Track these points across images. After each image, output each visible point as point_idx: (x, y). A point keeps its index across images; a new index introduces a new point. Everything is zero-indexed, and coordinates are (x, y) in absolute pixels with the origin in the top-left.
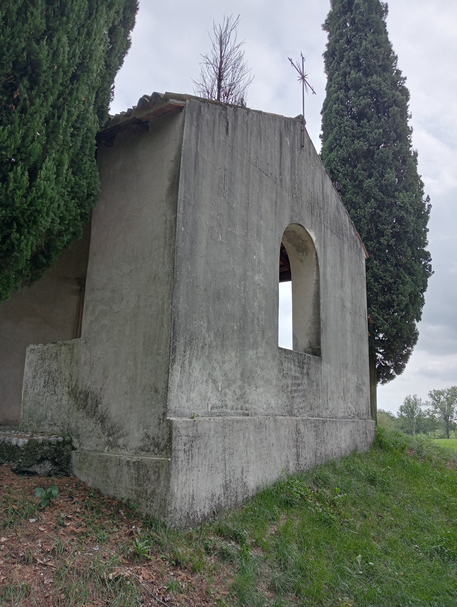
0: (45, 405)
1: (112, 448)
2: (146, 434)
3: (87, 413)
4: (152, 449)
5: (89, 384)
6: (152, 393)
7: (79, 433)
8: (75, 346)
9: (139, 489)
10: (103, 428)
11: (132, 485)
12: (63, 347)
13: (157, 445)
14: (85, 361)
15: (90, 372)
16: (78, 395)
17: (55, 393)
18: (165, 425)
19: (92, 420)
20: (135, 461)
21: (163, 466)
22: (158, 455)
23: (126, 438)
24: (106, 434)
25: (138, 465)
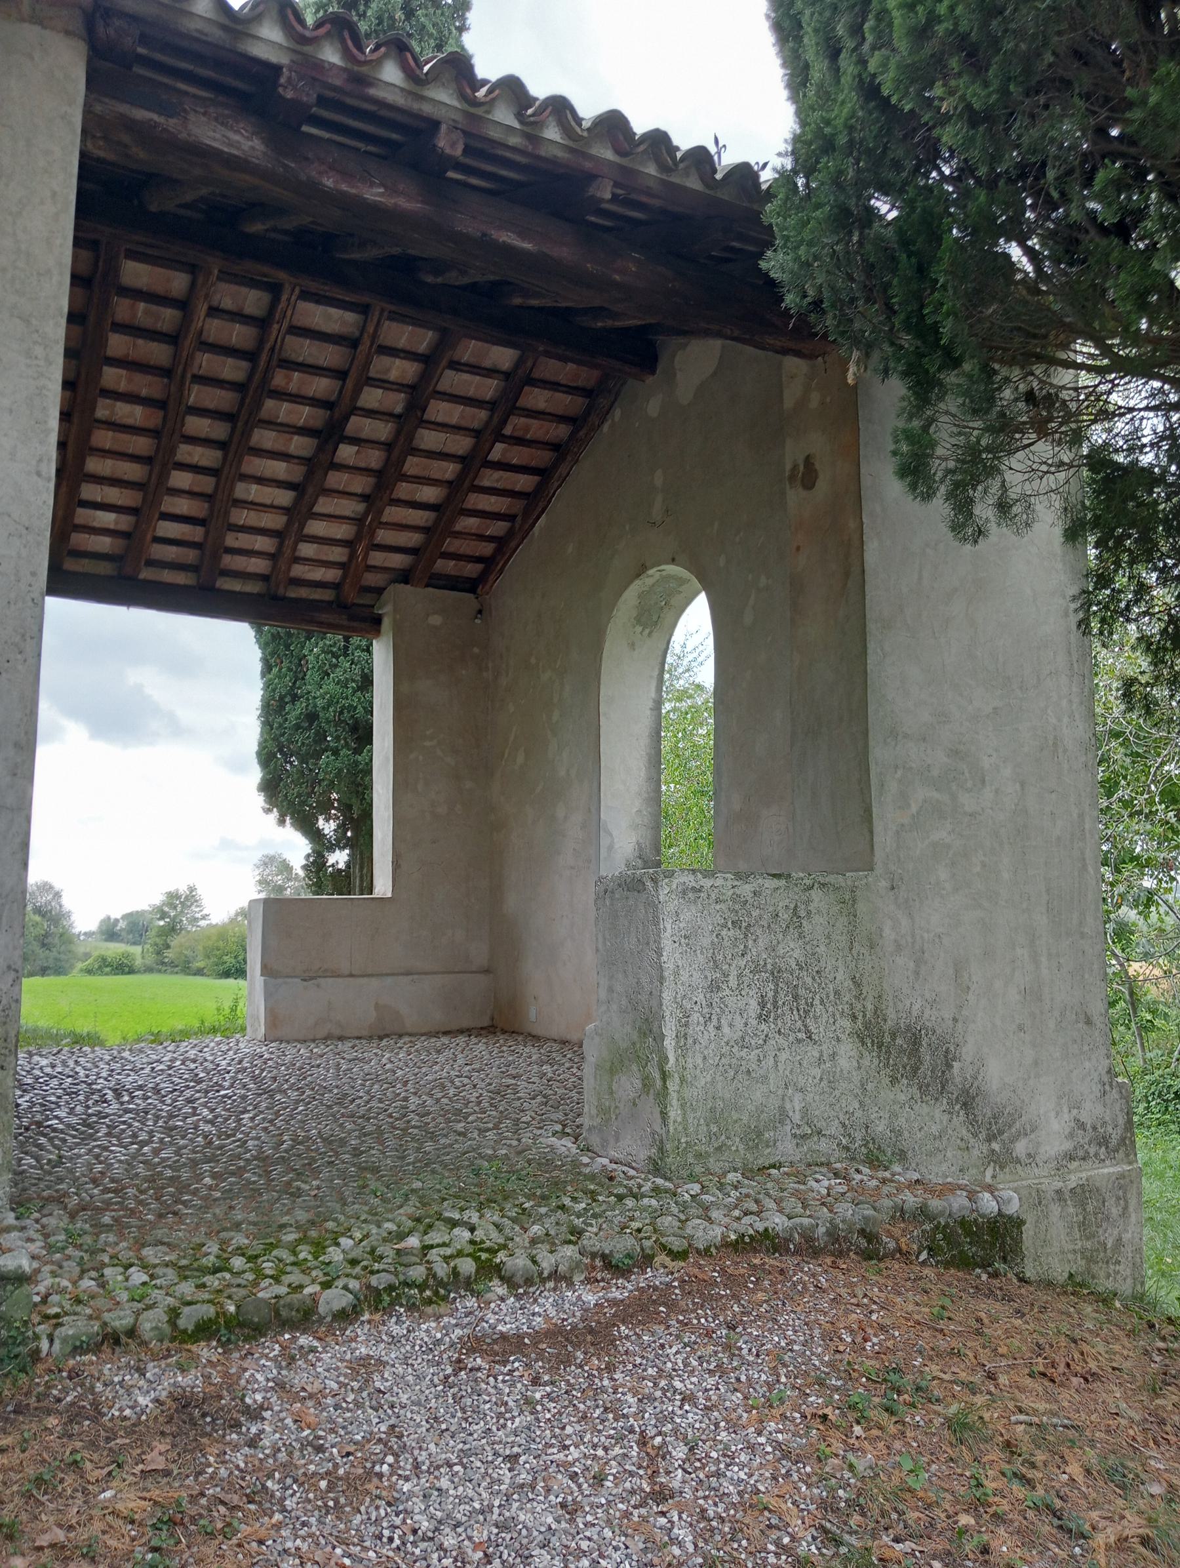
0: (772, 1076)
1: (1002, 1168)
2: (1077, 1120)
3: (923, 1088)
4: (1092, 1151)
5: (917, 1007)
6: (1080, 1025)
7: (905, 1145)
8: (858, 893)
9: (1088, 1245)
10: (972, 1122)
11: (1074, 1241)
12: (816, 894)
13: (1104, 1141)
14: (896, 941)
15: (917, 973)
16: (887, 1039)
17: (810, 1037)
18: (1115, 1094)
19: (938, 1104)
20: (1074, 1185)
21: (1132, 1182)
22: (1108, 1162)
23: (1033, 1136)
24: (982, 1136)
25: (1083, 1194)
